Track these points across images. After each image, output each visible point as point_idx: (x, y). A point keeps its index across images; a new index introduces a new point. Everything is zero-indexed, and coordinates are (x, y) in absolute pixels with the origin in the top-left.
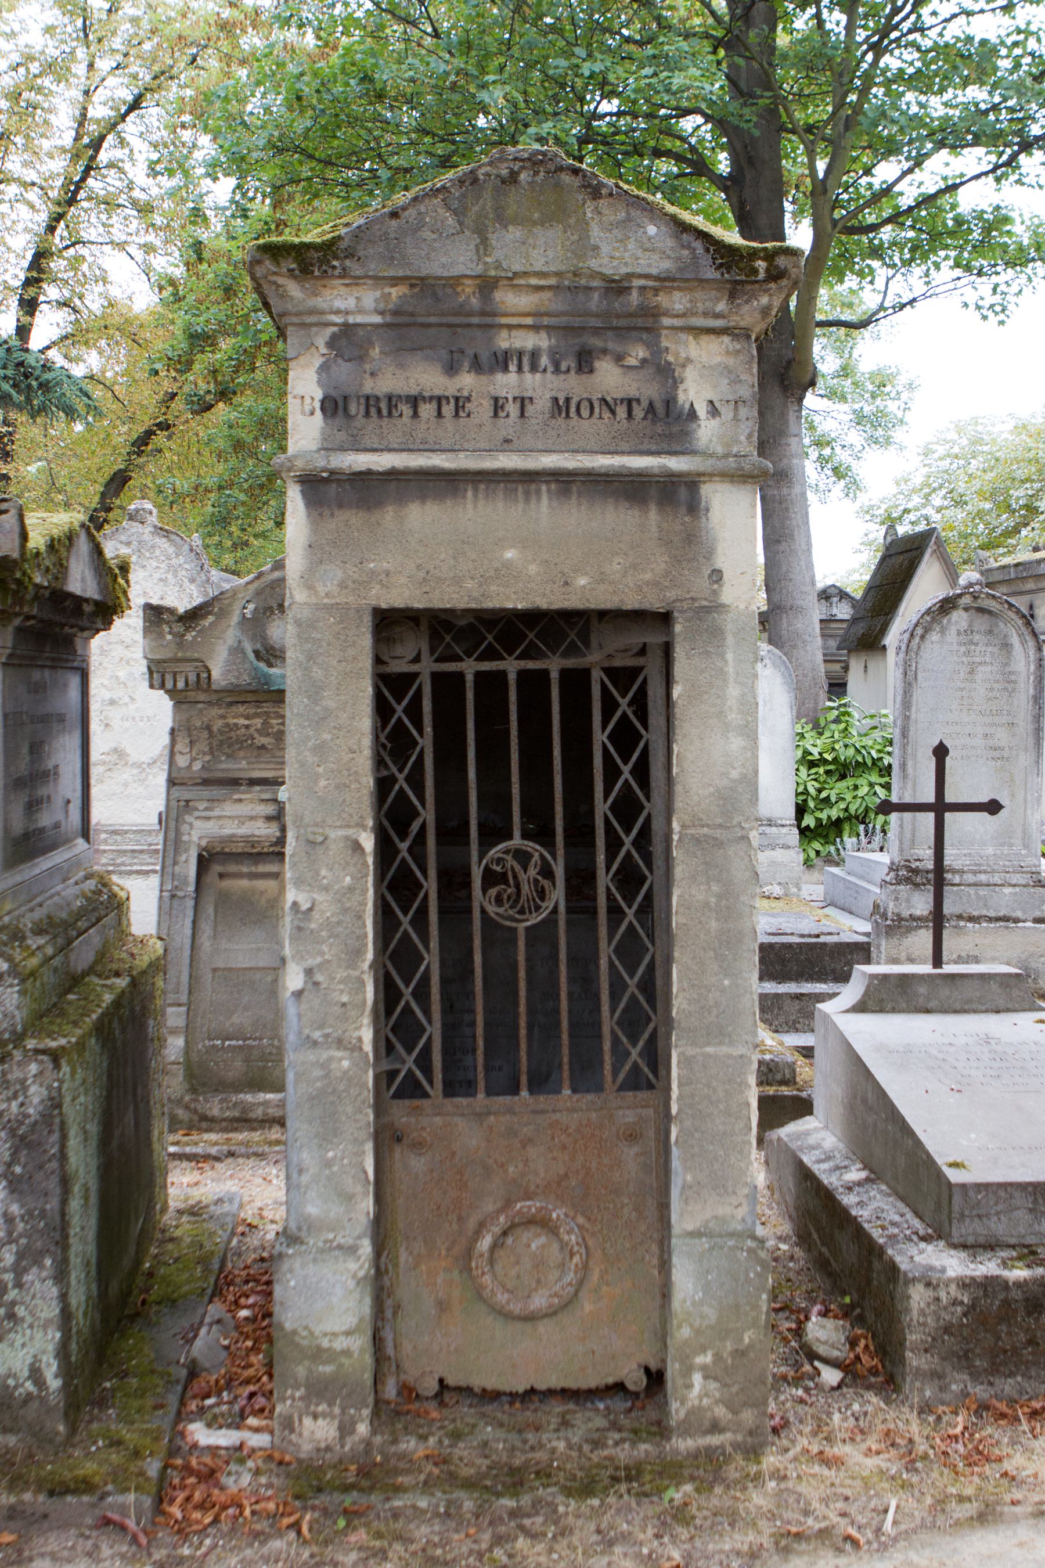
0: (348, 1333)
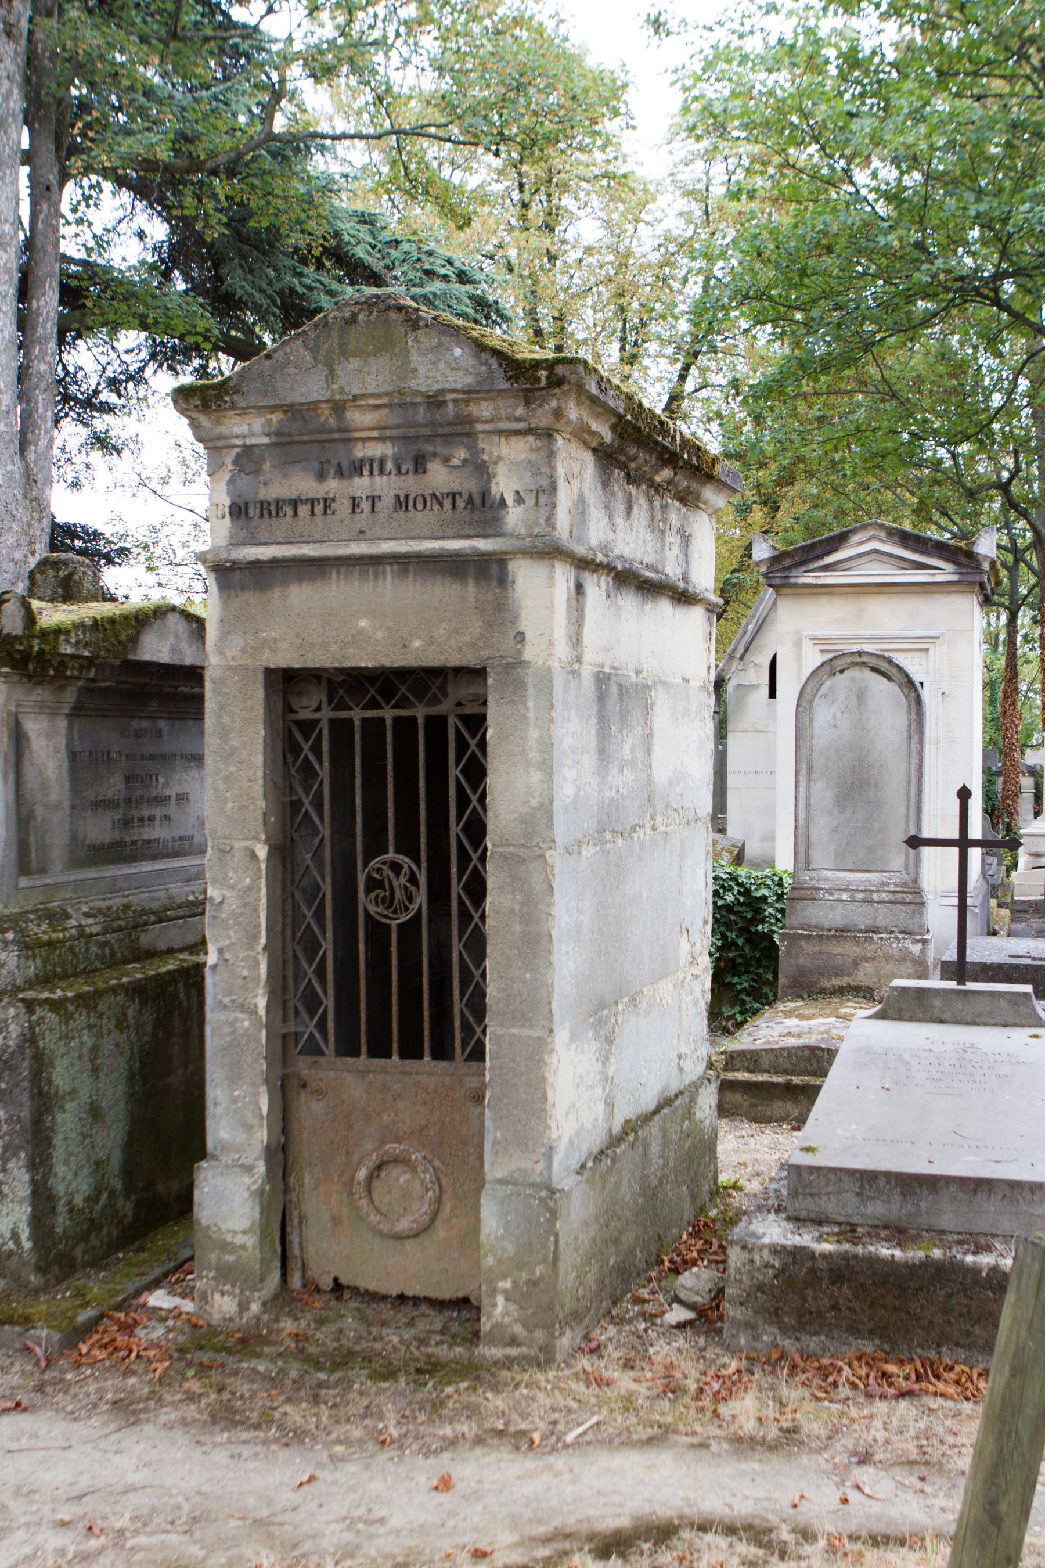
0: (244, 1232)
